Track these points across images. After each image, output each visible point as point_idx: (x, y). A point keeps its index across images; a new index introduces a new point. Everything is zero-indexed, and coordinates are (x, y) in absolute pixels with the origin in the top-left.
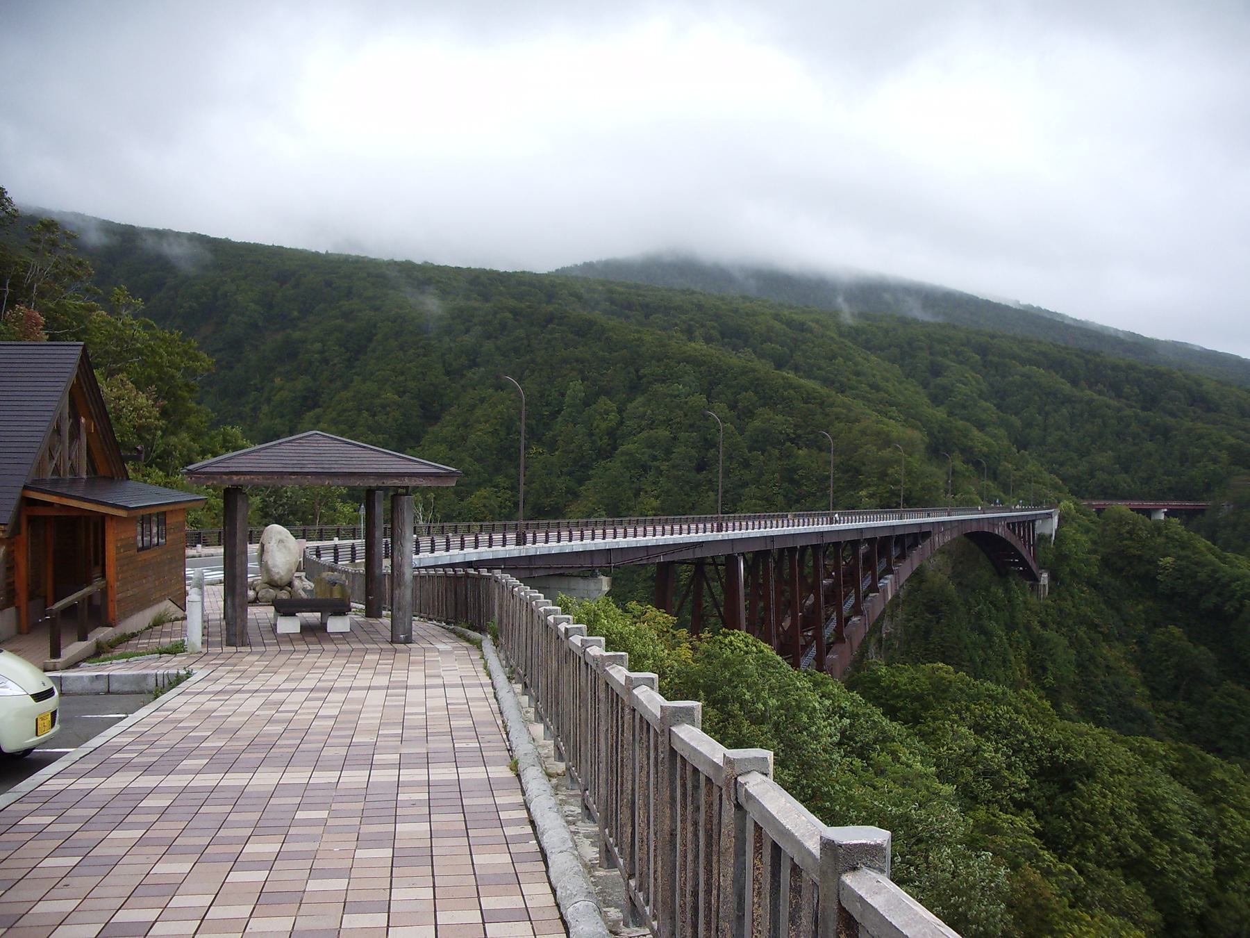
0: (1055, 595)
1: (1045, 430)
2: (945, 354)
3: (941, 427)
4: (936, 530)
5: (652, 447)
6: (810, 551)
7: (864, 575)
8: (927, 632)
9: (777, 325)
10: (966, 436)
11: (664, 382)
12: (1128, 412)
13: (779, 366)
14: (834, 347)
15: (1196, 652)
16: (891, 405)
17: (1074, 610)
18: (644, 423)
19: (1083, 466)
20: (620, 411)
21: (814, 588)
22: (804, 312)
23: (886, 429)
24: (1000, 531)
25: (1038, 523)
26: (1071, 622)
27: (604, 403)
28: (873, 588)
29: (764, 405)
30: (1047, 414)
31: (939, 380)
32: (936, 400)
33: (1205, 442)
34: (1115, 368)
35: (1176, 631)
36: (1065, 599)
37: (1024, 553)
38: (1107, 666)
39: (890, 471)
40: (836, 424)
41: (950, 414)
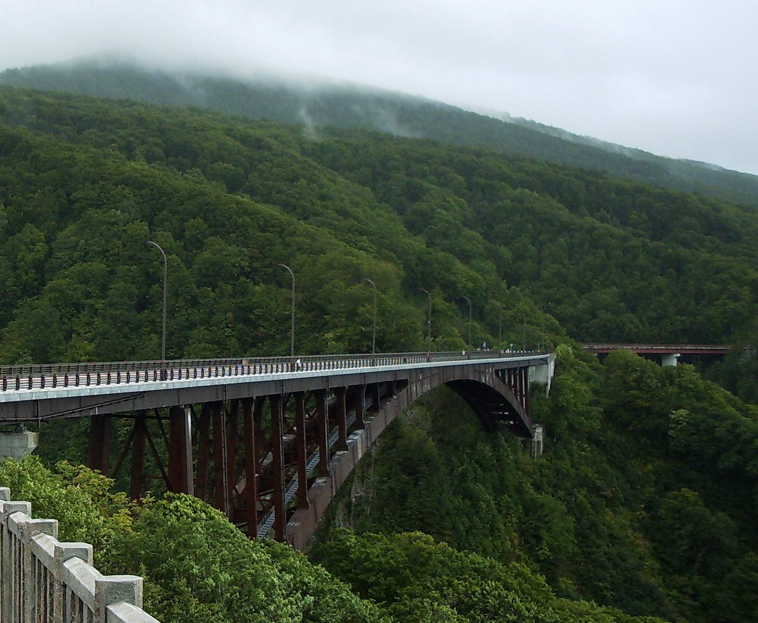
0: (551, 453)
1: (540, 263)
2: (424, 176)
3: (419, 259)
4: (414, 379)
5: (86, 282)
6: (267, 402)
7: (330, 430)
8: (404, 496)
9: (230, 142)
10: (448, 270)
11: (99, 207)
12: (635, 242)
13: (232, 189)
14: (296, 166)
15: (714, 519)
16: (361, 234)
17: (572, 471)
18: (76, 254)
19: (584, 304)
20: (49, 241)
21: (273, 445)
22: (260, 127)
23: (355, 261)
24: (487, 379)
25: (531, 370)
26: (569, 484)
27: (31, 231)
28: (341, 445)
29: (214, 234)
30: (542, 244)
31: (418, 206)
32: (413, 228)
33: (724, 276)
34: (620, 191)
35: (691, 495)
36: (561, 458)
37: (515, 404)
38: (611, 536)
39: (361, 310)
40: (298, 255)
41: (430, 244)
